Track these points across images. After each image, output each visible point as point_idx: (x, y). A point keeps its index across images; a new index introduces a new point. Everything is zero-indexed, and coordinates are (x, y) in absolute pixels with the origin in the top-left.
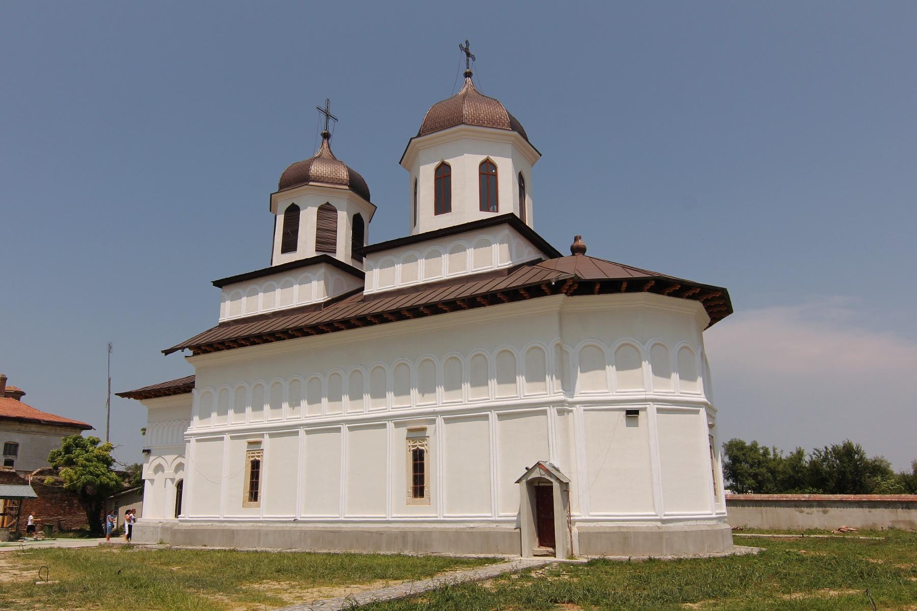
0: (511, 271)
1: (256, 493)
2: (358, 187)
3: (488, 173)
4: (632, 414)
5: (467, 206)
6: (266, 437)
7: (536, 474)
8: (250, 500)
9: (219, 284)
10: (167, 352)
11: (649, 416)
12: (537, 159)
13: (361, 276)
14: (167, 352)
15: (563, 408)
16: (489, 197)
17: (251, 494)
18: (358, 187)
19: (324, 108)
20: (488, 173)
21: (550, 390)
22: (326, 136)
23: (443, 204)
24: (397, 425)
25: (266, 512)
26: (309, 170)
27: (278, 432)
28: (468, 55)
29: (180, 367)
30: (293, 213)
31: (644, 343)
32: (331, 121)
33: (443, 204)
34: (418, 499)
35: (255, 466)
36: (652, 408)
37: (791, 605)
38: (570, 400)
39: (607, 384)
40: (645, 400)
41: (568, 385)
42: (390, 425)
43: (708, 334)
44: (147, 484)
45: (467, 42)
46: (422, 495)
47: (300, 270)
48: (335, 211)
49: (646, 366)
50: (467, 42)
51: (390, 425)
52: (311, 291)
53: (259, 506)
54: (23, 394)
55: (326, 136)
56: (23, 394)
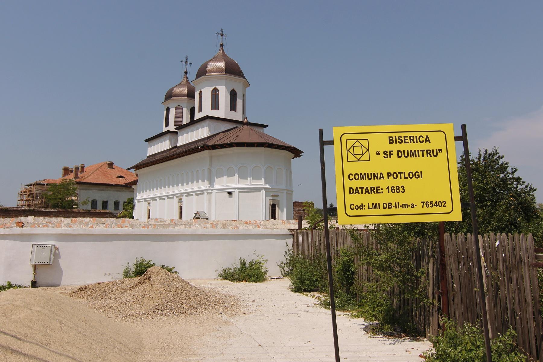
0: (208, 138)
4: (230, 193)
6: (184, 196)
9: (146, 141)
11: (236, 194)
15: (209, 192)
18: (233, 70)
20: (215, 94)
21: (203, 185)
24: (177, 197)
25: (285, 241)
26: (172, 92)
27: (189, 194)
30: (168, 110)
36: (236, 191)
38: (211, 188)
39: (223, 182)
40: (234, 188)
41: (211, 183)
47: (163, 137)
48: (182, 108)
49: (236, 176)
55: (222, 45)
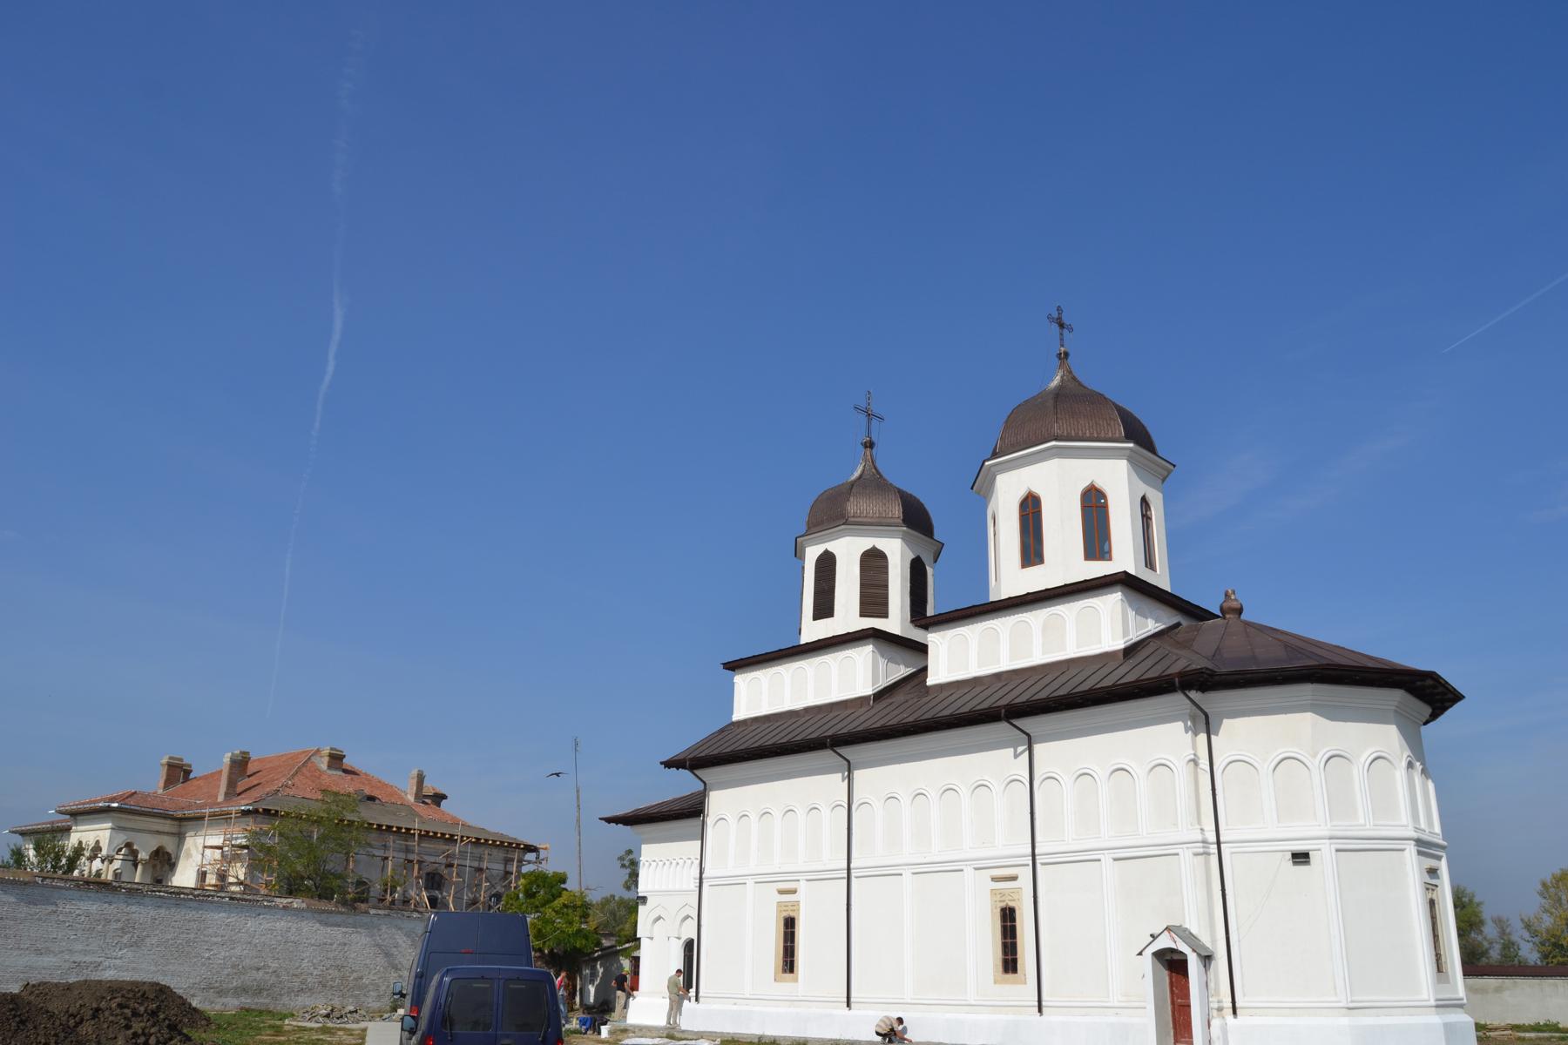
1: (792, 963)
2: (916, 519)
3: (1094, 504)
4: (1301, 858)
5: (1065, 559)
7: (1165, 942)
8: (784, 971)
10: (789, 962)
12: (1169, 472)
13: (922, 649)
14: (789, 962)
16: (1096, 541)
17: (785, 962)
19: (863, 405)
20: (1094, 504)
22: (870, 445)
23: (1032, 553)
28: (1062, 326)
29: (682, 784)
31: (1314, 756)
32: (874, 422)
33: (1032, 553)
34: (1010, 976)
35: (790, 924)
37: (262, 1042)
42: (969, 871)
43: (1426, 730)
44: (644, 943)
45: (1059, 308)
46: (1015, 970)
50: (1059, 308)
51: (969, 871)
52: (853, 676)
53: (796, 980)
54: (444, 797)
56: (444, 797)
